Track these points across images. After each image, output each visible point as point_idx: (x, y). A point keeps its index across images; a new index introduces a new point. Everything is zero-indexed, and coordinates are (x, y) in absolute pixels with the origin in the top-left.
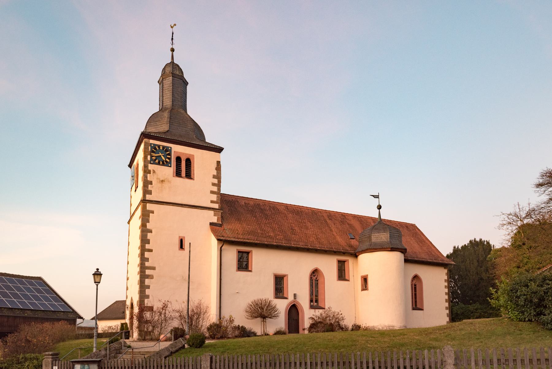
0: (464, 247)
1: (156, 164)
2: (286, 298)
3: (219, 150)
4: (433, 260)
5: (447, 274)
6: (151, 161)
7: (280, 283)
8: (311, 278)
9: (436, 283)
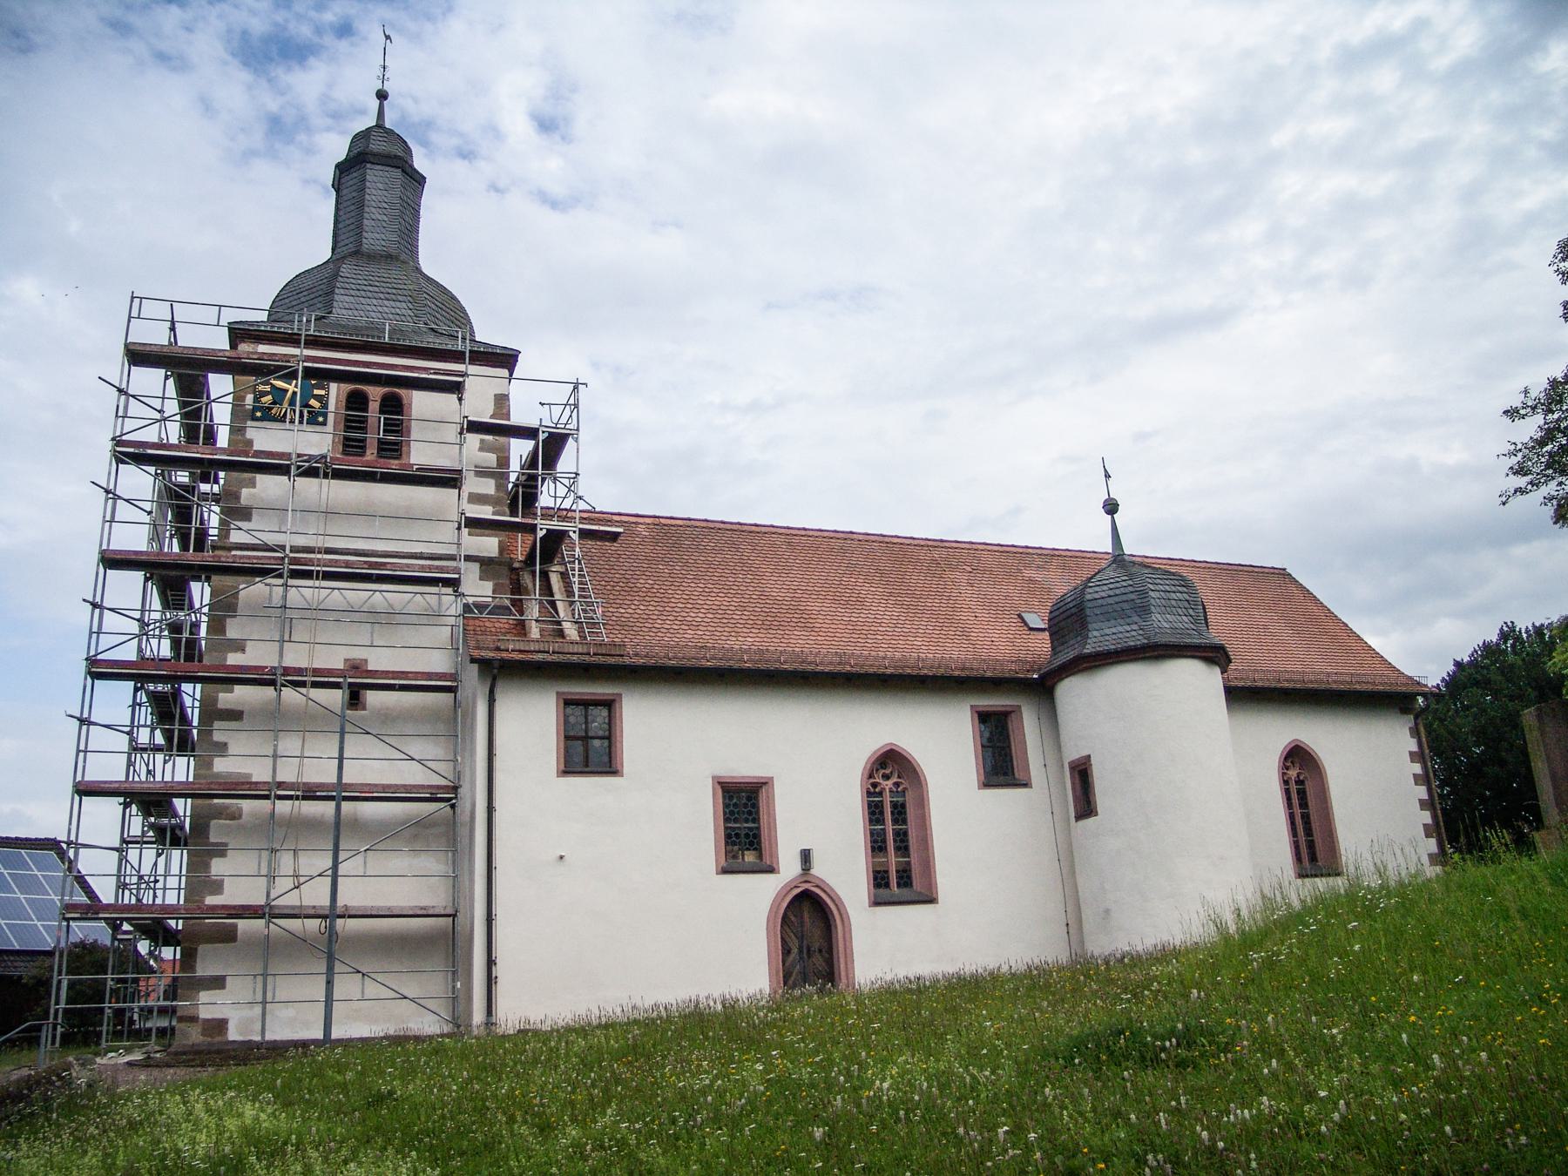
0: (1473, 663)
2: (771, 870)
3: (505, 359)
5: (1415, 732)
6: (255, 409)
7: (743, 818)
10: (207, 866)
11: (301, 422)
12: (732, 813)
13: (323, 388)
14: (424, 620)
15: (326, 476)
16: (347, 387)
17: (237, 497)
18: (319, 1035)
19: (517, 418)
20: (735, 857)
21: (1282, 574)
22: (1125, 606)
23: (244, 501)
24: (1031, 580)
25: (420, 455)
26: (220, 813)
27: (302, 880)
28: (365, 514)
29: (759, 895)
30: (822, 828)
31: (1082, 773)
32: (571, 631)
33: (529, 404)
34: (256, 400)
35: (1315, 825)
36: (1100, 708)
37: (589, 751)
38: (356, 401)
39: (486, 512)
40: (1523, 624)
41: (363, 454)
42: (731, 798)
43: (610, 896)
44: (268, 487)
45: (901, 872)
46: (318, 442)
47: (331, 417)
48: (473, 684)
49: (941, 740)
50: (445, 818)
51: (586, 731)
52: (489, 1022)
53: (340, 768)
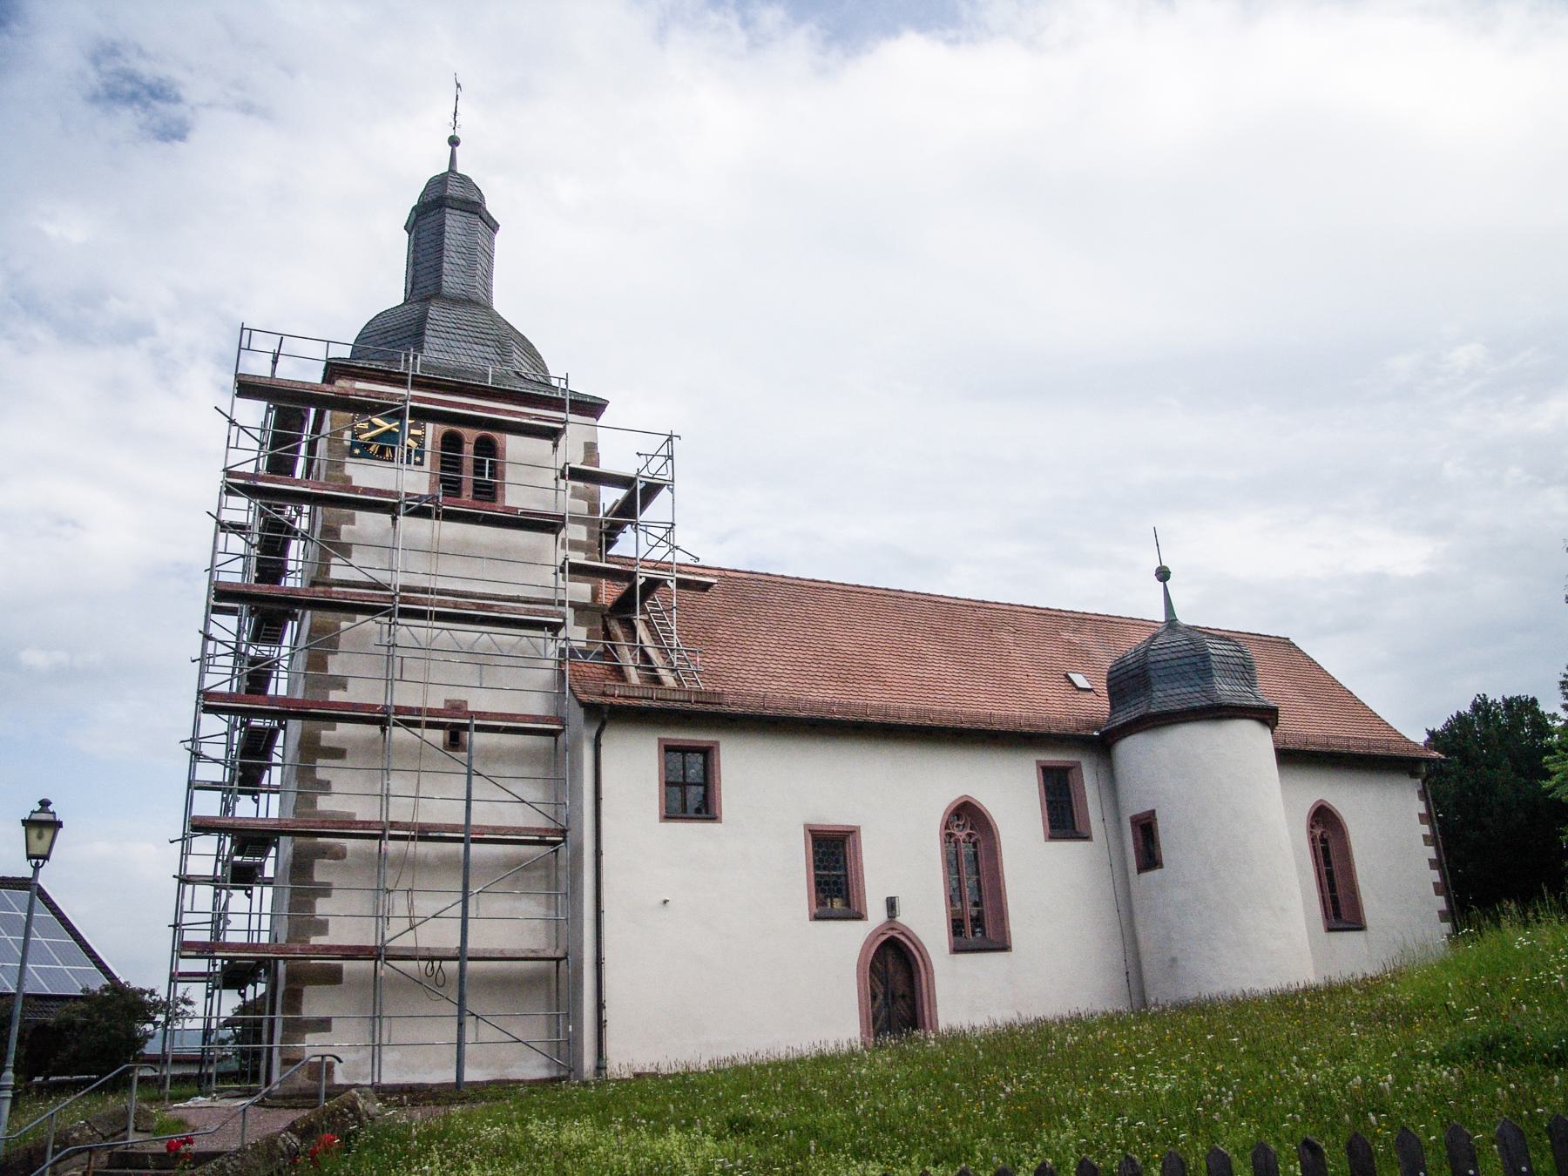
1: (371, 457)
2: (860, 917)
3: (591, 407)
4: (1378, 761)
5: (1423, 795)
6: (354, 445)
7: (833, 865)
8: (950, 835)
9: (1391, 832)
10: (312, 906)
11: (409, 462)
12: (821, 860)
13: (419, 428)
14: (521, 662)
15: (437, 518)
16: (444, 428)
17: (336, 533)
18: (451, 1077)
19: (606, 465)
20: (825, 904)
21: (1286, 643)
22: (1187, 668)
23: (344, 538)
24: (1069, 642)
25: (515, 497)
26: (324, 852)
27: (417, 921)
28: (464, 553)
29: (848, 942)
30: (906, 877)
31: (1146, 828)
32: (669, 679)
33: (619, 454)
34: (354, 436)
35: (1338, 881)
36: (1162, 764)
37: (691, 796)
38: (451, 443)
39: (579, 558)
40: (1496, 695)
41: (459, 495)
42: (820, 846)
43: (711, 942)
44: (369, 524)
45: (979, 924)
46: (416, 481)
47: (428, 456)
48: (579, 728)
49: (1009, 791)
50: (556, 857)
51: (684, 776)
52: (600, 1067)
53: (468, 808)
